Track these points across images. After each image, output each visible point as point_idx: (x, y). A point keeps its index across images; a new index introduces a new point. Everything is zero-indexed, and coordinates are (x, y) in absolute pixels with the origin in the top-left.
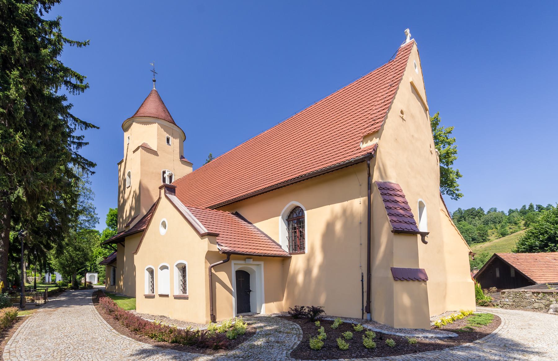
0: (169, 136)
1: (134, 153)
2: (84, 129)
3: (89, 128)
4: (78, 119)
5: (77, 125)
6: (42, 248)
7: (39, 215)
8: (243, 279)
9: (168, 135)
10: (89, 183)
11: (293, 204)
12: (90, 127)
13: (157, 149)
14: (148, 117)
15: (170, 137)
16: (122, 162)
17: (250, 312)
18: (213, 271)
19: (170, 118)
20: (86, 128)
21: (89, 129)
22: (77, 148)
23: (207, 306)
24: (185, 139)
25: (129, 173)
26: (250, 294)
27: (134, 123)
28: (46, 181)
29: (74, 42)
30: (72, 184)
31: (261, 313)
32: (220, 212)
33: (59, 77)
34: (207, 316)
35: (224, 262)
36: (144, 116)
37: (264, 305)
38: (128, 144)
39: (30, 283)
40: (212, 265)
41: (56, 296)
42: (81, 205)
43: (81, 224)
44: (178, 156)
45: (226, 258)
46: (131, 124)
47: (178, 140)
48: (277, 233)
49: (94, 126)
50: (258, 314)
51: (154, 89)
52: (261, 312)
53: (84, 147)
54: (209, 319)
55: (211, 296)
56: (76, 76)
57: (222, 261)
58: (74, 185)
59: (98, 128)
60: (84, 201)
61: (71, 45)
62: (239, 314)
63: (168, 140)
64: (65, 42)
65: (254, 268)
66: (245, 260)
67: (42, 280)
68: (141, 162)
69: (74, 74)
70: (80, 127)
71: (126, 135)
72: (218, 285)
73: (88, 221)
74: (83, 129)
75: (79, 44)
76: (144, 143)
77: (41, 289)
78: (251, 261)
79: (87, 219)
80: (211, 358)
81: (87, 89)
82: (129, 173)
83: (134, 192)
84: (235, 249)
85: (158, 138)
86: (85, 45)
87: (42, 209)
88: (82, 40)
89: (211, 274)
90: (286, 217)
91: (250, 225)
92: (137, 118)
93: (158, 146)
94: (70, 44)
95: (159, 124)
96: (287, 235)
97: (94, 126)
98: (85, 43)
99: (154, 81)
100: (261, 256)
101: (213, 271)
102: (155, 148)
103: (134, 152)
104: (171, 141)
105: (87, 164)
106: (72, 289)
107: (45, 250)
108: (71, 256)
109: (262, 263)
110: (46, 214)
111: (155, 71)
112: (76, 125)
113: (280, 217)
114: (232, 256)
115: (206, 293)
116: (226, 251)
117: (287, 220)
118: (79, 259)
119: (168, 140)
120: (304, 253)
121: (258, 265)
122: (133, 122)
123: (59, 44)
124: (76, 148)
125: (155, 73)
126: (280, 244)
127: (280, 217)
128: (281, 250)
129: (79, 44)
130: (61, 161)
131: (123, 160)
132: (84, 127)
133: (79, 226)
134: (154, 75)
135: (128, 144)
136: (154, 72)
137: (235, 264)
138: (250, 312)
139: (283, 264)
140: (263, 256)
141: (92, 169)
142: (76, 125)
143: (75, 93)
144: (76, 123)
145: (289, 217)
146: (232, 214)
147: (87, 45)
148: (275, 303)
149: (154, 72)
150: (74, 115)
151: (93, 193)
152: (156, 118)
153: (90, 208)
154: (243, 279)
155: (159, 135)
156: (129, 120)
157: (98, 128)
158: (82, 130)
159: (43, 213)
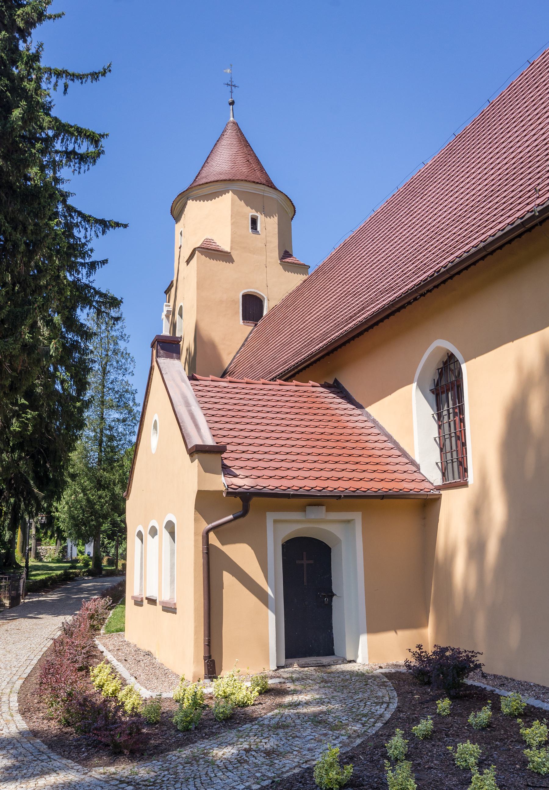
0: (256, 214)
1: (187, 264)
2: (100, 235)
3: (108, 229)
4: (90, 216)
5: (89, 229)
6: (31, 486)
7: (14, 421)
8: (312, 562)
9: (253, 213)
10: (126, 338)
11: (438, 348)
12: (110, 229)
13: (231, 248)
14: (214, 182)
15: (258, 214)
16: (171, 288)
17: (333, 654)
18: (213, 539)
19: (258, 173)
20: (104, 232)
21: (110, 232)
22: (88, 275)
23: (196, 633)
24: (295, 211)
25: (181, 307)
26: (333, 604)
27: (190, 202)
28: (7, 353)
29: (87, 75)
30: (51, 353)
31: (359, 660)
32: (292, 386)
33: (35, 153)
34: (196, 661)
35: (235, 518)
36: (207, 183)
37: (364, 639)
38: (180, 248)
39: (41, 560)
40: (210, 526)
41: (47, 592)
42: (110, 389)
43: (111, 428)
44: (275, 255)
45: (239, 509)
46: (185, 204)
47: (276, 219)
48: (410, 431)
49: (118, 225)
50: (350, 662)
51: (232, 119)
52: (357, 656)
53: (100, 271)
54: (202, 670)
55: (207, 608)
56: (87, 137)
57: (231, 517)
58: (54, 355)
59: (125, 226)
60: (116, 378)
61: (82, 83)
62: (290, 661)
63: (254, 222)
64: (73, 80)
65: (336, 530)
66: (303, 509)
67: (61, 552)
68: (198, 283)
69: (85, 135)
70: (93, 233)
71: (178, 227)
72: (227, 578)
73: (124, 420)
74: (99, 233)
75: (95, 76)
76: (207, 241)
77: (39, 575)
78: (320, 513)
79: (121, 417)
80: (72, 776)
81: (102, 156)
82: (181, 307)
83: (187, 350)
84: (262, 483)
85: (232, 224)
86: (104, 74)
87: (23, 406)
88: (98, 68)
89: (208, 549)
90: (429, 385)
91: (358, 411)
92: (194, 189)
93: (232, 242)
94: (80, 81)
95: (235, 192)
96: (437, 435)
97: (118, 225)
98: (105, 71)
99: (232, 103)
100: (340, 497)
101: (213, 539)
102: (226, 247)
103: (188, 262)
104: (261, 224)
105: (104, 303)
106: (88, 576)
107: (36, 491)
108: (88, 500)
109: (357, 517)
110: (29, 416)
111: (233, 84)
112: (86, 229)
113: (414, 385)
114: (254, 501)
115: (195, 600)
116: (240, 490)
117: (432, 391)
118: (102, 507)
119: (254, 222)
120: (465, 484)
121: (348, 521)
122: (188, 199)
123: (37, 94)
124: (87, 274)
125: (233, 87)
126: (418, 460)
127: (414, 385)
128: (416, 476)
129: (95, 76)
130: (35, 309)
131: (172, 282)
132: (101, 229)
133: (108, 432)
134: (231, 92)
135: (180, 248)
136: (231, 85)
137: (275, 521)
138: (333, 654)
139: (424, 518)
140: (345, 497)
141: (113, 313)
142: (86, 229)
143: (82, 170)
144: (87, 226)
145: (437, 385)
146: (322, 386)
147: (108, 74)
148: (400, 633)
149: (231, 85)
150: (83, 212)
151: (132, 360)
152: (230, 180)
153: (127, 391)
154: (312, 562)
155: (235, 215)
156: (180, 197)
157: (125, 226)
158: (97, 236)
159: (23, 415)
